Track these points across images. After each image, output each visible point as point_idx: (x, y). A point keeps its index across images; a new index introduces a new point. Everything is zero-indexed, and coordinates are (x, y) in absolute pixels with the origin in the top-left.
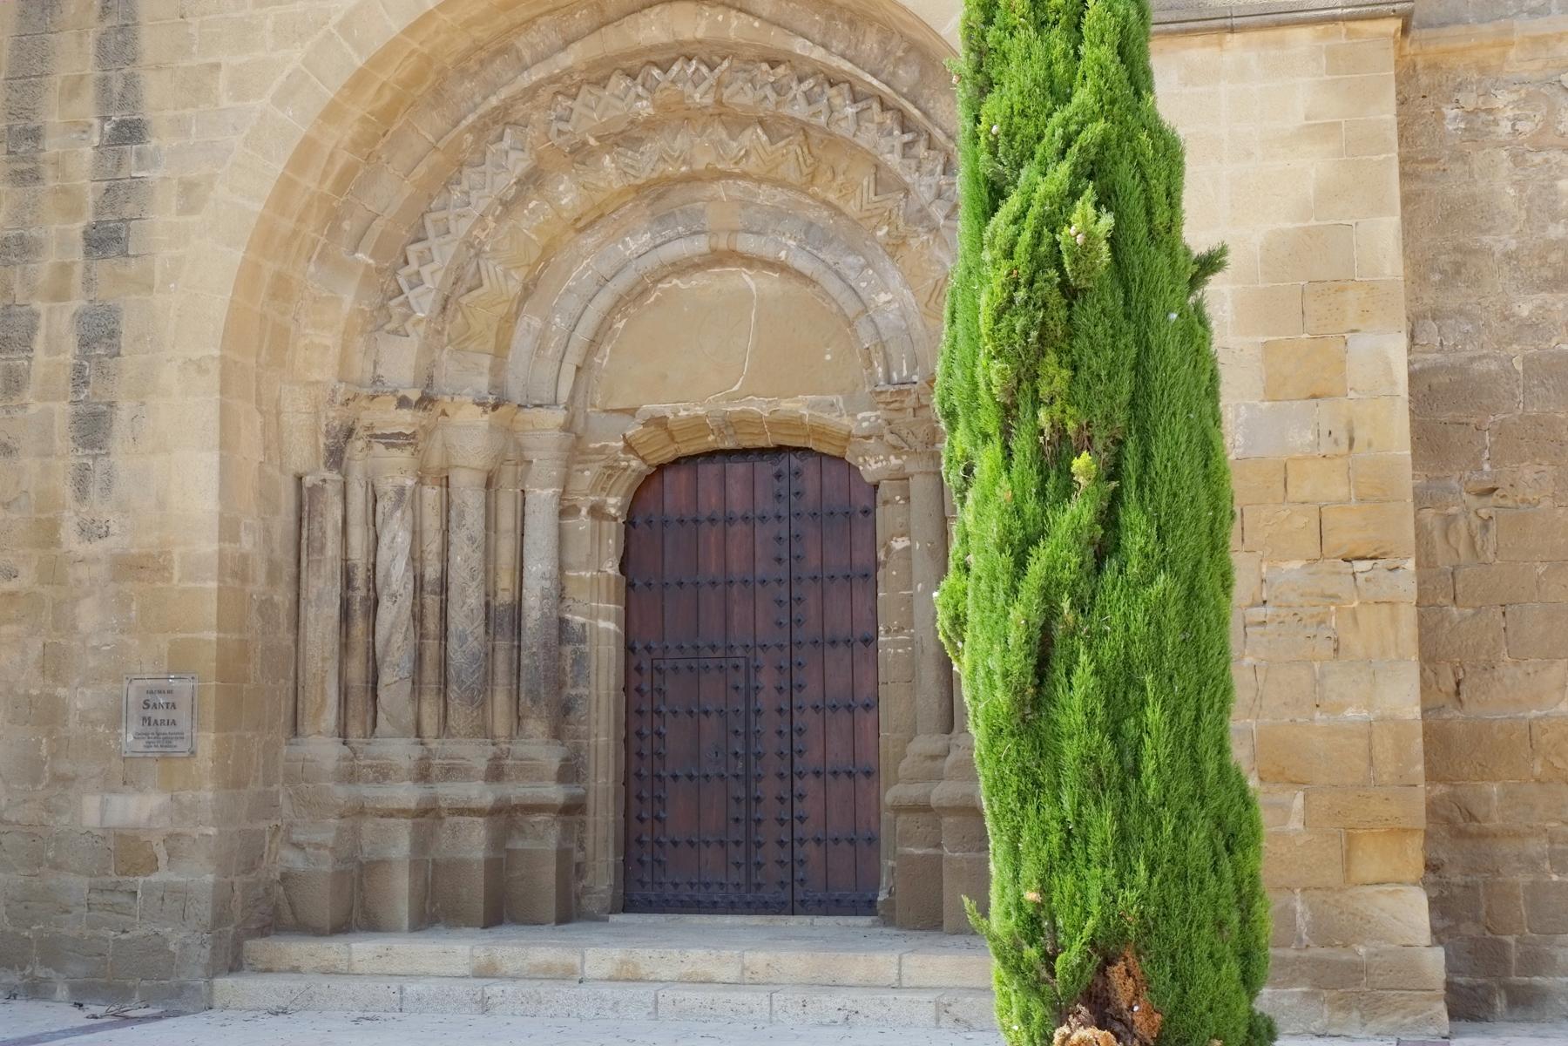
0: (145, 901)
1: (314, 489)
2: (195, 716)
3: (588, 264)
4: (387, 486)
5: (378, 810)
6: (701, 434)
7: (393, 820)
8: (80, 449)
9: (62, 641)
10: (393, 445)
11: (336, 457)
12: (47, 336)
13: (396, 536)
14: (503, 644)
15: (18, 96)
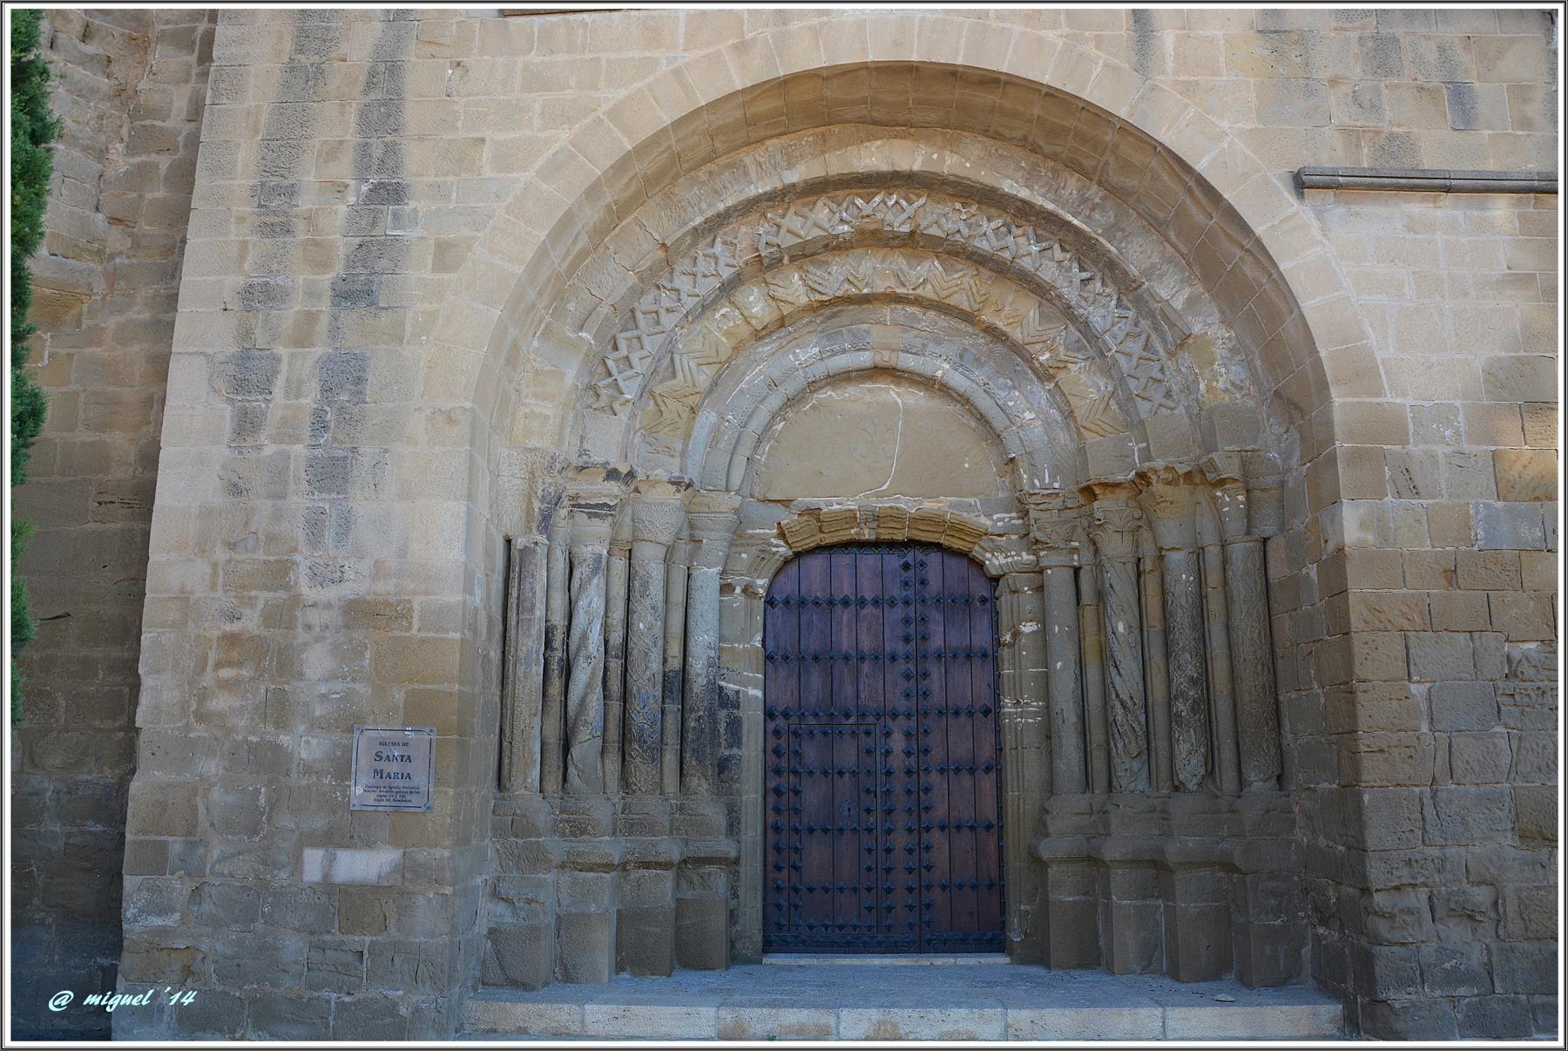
0: (372, 961)
1: (525, 551)
3: (760, 370)
5: (578, 864)
6: (847, 526)
7: (591, 875)
8: (316, 493)
10: (596, 515)
11: (546, 522)
13: (591, 602)
14: (673, 707)
15: (275, 155)
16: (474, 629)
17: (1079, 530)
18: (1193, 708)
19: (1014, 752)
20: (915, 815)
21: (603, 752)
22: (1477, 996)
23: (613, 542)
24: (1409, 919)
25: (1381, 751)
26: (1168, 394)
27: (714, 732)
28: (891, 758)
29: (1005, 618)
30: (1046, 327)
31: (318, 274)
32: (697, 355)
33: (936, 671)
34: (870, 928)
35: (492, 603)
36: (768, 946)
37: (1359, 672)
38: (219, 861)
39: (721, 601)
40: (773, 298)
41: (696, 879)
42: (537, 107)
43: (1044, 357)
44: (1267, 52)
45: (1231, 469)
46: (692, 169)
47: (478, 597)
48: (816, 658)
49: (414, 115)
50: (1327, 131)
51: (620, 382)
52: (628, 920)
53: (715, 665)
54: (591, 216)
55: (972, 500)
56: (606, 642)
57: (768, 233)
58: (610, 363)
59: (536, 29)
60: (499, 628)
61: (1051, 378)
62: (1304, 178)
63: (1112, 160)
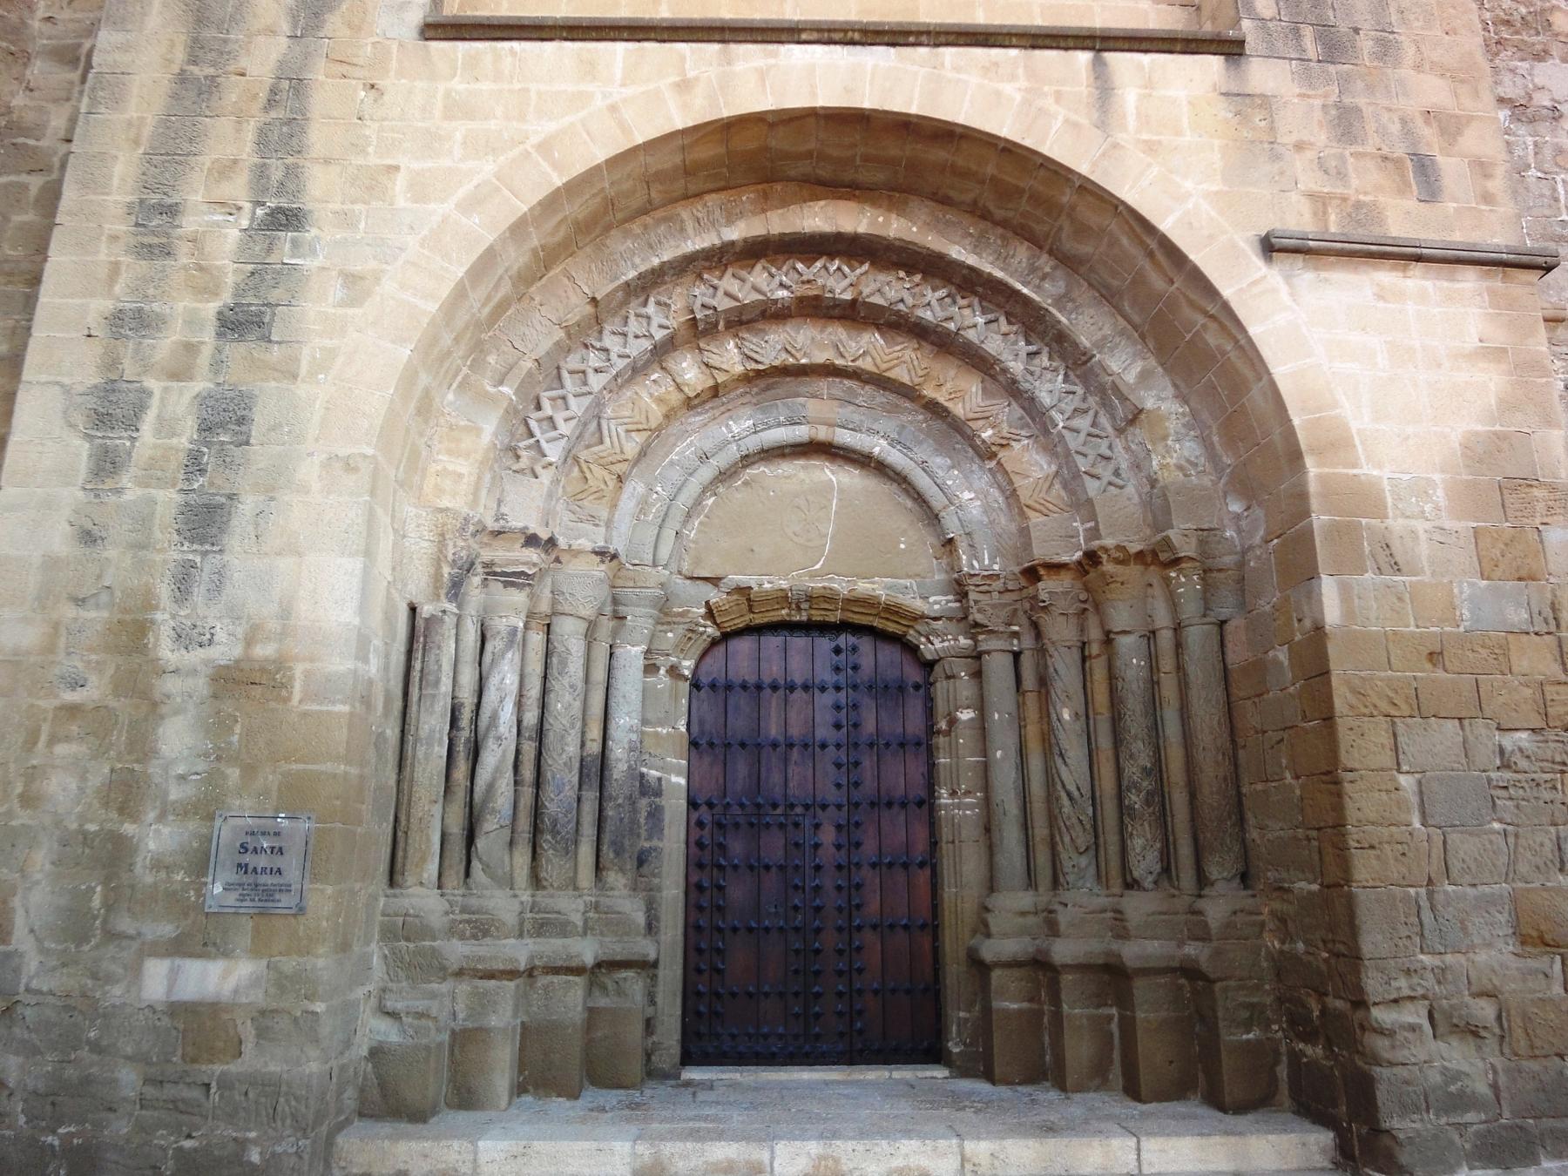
0: (221, 1097)
2: (308, 865)
4: (500, 624)
7: (493, 982)
8: (187, 544)
9: (137, 767)
10: (513, 584)
11: (456, 589)
12: (159, 417)
13: (505, 678)
14: (590, 795)
15: (158, 170)
16: (366, 701)
17: (1020, 613)
18: (1147, 800)
19: (950, 846)
20: (846, 912)
21: (511, 843)
22: (1485, 1122)
23: (530, 615)
24: (1410, 1035)
25: (1372, 847)
26: (1117, 473)
27: (634, 822)
28: (820, 851)
29: (941, 707)
30: (988, 403)
31: (201, 301)
32: (626, 420)
33: (868, 762)
34: (796, 1037)
35: (391, 675)
36: (688, 1059)
37: (1345, 759)
38: (37, 974)
39: (644, 682)
40: (707, 365)
41: (610, 986)
42: (458, 136)
43: (987, 434)
44: (1231, 115)
45: (1187, 548)
46: (626, 221)
47: (373, 668)
48: (743, 745)
49: (318, 137)
50: (1294, 196)
51: (544, 444)
52: (531, 1036)
53: (637, 749)
54: (516, 258)
55: (907, 582)
56: (519, 722)
57: (704, 295)
58: (533, 424)
59: (460, 56)
60: (398, 704)
61: (993, 456)
62: (1273, 240)
63: (1066, 225)
